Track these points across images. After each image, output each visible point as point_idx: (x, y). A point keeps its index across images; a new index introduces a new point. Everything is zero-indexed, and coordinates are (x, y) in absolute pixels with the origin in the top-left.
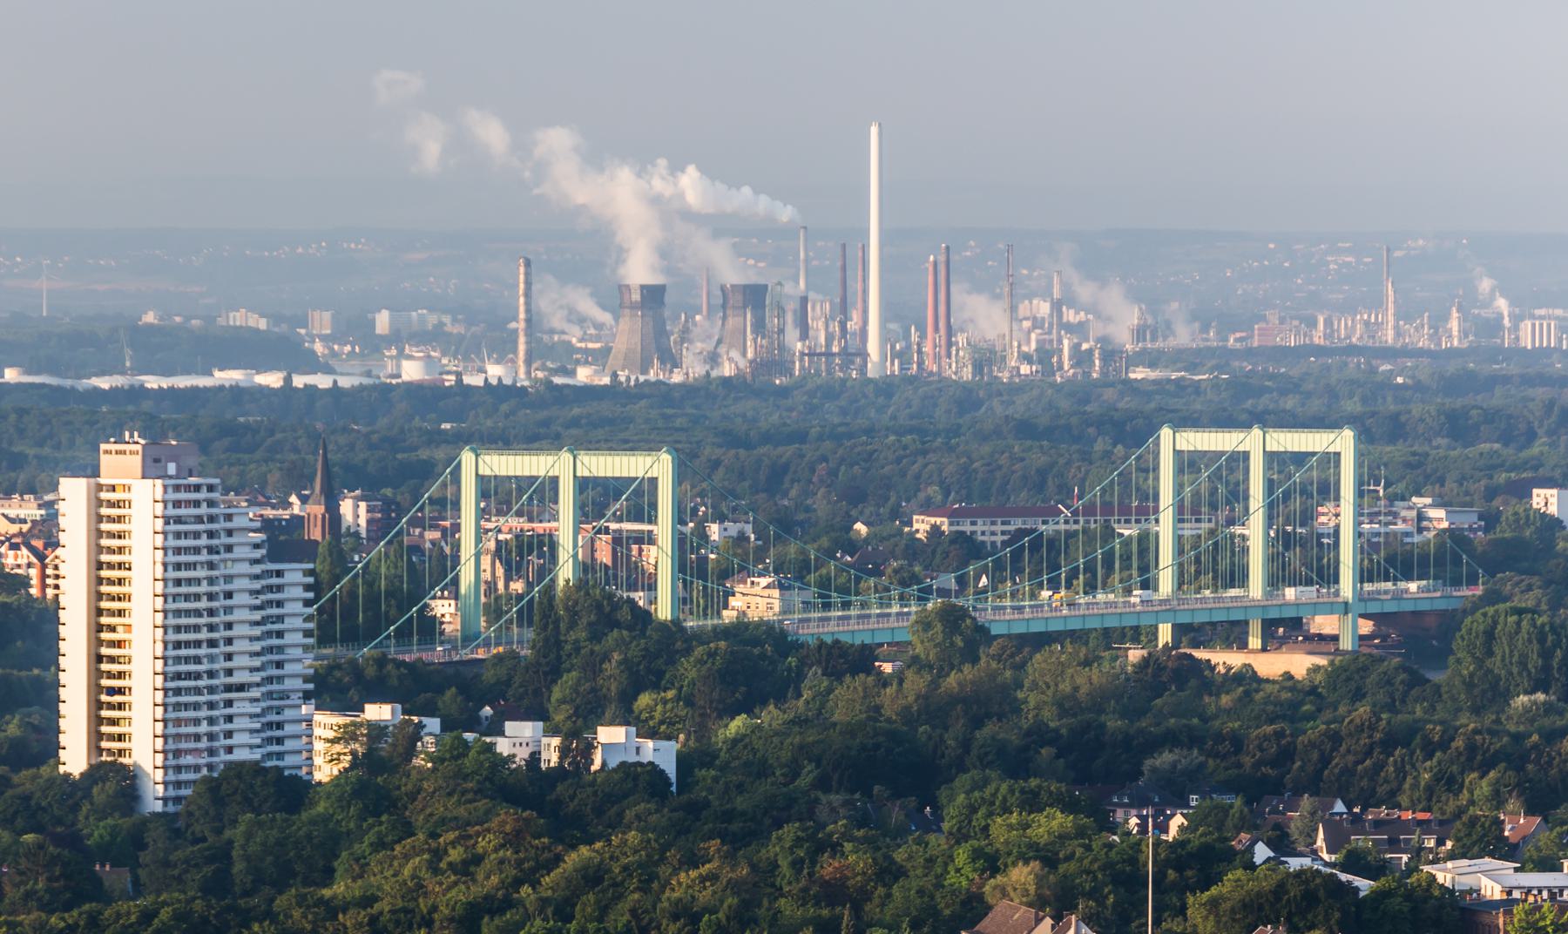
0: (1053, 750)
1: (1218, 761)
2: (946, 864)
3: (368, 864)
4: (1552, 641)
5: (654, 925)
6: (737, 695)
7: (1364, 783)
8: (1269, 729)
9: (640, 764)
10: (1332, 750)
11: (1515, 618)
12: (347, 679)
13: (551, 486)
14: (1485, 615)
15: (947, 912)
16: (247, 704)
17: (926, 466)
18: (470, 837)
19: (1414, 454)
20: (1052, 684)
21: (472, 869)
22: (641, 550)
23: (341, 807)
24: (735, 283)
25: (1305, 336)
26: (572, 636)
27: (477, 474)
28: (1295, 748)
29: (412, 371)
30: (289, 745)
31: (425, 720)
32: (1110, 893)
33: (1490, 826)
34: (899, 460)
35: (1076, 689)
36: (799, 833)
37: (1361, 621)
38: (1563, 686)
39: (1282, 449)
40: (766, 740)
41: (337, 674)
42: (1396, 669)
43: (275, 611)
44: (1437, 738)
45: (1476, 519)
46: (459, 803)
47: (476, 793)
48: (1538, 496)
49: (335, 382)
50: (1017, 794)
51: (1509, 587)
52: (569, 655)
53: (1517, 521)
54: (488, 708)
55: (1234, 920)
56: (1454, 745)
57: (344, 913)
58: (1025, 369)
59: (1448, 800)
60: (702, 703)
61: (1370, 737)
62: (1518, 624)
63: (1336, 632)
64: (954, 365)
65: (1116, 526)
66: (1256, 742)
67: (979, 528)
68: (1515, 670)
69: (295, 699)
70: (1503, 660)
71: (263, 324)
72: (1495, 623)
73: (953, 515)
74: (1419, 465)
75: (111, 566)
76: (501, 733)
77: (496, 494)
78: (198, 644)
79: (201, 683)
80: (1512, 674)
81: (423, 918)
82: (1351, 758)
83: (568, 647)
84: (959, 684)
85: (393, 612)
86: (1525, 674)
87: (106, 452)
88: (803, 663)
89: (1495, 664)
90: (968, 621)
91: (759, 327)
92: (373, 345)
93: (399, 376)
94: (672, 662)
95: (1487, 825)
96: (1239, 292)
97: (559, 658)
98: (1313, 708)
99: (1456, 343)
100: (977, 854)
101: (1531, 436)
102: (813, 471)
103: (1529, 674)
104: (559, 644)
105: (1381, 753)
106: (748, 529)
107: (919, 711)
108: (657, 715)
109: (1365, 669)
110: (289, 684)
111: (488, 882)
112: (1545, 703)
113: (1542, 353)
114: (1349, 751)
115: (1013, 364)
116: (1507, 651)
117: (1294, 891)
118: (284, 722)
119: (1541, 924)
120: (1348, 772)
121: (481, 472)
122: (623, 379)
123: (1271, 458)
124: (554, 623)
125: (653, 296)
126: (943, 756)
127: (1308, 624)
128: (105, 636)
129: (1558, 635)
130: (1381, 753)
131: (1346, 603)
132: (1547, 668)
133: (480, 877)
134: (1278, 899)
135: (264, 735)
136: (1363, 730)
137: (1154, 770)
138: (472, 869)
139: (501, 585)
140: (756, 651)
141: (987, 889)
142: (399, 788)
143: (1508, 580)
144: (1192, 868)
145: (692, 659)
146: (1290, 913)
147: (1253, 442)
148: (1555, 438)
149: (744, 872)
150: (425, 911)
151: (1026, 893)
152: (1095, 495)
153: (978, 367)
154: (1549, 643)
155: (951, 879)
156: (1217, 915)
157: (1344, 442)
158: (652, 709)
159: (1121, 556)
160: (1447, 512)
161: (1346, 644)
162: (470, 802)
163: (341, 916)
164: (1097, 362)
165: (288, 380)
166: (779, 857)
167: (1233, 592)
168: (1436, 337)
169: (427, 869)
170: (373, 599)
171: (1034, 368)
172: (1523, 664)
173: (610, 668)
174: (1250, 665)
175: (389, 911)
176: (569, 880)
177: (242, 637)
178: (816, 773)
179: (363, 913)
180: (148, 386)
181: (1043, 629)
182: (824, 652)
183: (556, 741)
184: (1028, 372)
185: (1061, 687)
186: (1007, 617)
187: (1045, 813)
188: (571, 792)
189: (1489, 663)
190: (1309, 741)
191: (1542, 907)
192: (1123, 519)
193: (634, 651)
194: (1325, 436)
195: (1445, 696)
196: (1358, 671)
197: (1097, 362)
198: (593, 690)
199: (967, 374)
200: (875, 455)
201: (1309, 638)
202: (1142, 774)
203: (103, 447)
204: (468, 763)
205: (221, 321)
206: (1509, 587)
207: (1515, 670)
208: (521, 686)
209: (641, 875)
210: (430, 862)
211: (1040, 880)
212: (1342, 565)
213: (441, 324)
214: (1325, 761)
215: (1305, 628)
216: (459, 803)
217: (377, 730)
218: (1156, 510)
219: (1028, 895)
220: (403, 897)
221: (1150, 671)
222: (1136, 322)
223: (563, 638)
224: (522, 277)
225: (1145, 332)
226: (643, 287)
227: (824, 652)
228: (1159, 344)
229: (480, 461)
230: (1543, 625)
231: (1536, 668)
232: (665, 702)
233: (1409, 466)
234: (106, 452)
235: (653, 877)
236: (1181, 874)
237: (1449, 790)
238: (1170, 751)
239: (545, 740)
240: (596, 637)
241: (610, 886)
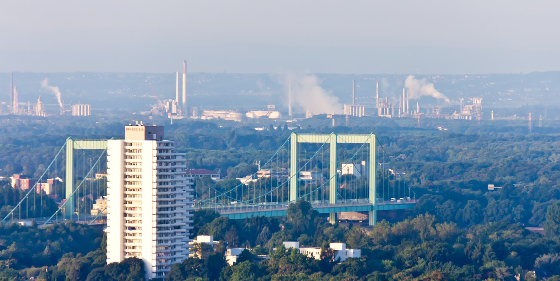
0: (516, 253)
16: (181, 234)
22: (41, 185)
23: (246, 275)
27: (73, 149)
39: (344, 142)
75: (130, 177)
78: (167, 209)
79: (168, 225)
87: (128, 129)
113: (82, 119)
121: (75, 148)
128: (128, 205)
131: (372, 206)
137: (540, 262)
147: (331, 139)
167: (366, 199)
177: (179, 207)
181: (233, 218)
182: (259, 221)
203: (126, 127)
227: (259, 221)
229: (75, 143)
234: (128, 129)
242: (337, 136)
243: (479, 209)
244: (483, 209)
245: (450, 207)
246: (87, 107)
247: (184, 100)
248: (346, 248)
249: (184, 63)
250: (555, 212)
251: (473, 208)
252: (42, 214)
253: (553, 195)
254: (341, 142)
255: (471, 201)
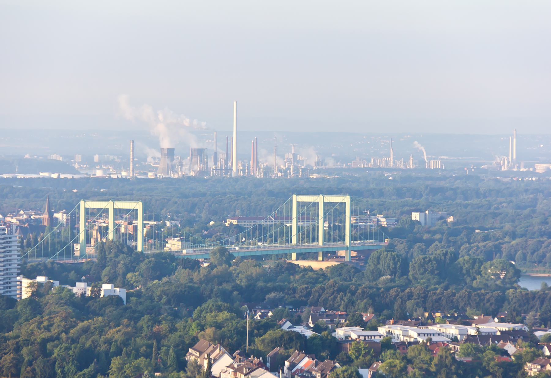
0: (238, 292)
1: (288, 296)
2: (190, 328)
3: (22, 326)
4: (397, 260)
5: (98, 345)
6: (157, 274)
7: (331, 303)
8: (304, 286)
9: (115, 296)
10: (322, 293)
11: (386, 253)
12: (42, 268)
13: (106, 211)
14: (377, 252)
15: (187, 342)
17: (237, 204)
18: (52, 318)
19: (382, 201)
20: (245, 272)
21: (50, 328)
24: (195, 148)
25: (366, 165)
26: (110, 256)
28: (311, 292)
29: (99, 173)
30: (13, 289)
31: (55, 282)
32: (235, 337)
33: (359, 317)
34: (229, 202)
35: (252, 274)
36: (149, 318)
37: (352, 252)
38: (400, 273)
40: (156, 288)
41: (39, 266)
42: (351, 268)
43: (8, 249)
44: (353, 289)
45: (395, 221)
46: (59, 306)
47: (64, 304)
48: (414, 214)
49: (73, 177)
50: (215, 307)
51: (396, 242)
52: (108, 262)
53: (404, 222)
54: (84, 277)
55: (269, 345)
56: (358, 291)
57: (9, 341)
58: (279, 174)
59: (351, 308)
60: (145, 276)
61: (333, 289)
62: (387, 255)
63: (344, 255)
64: (258, 173)
65: (284, 223)
66: (300, 290)
67: (246, 223)
68: (386, 268)
69: (15, 275)
70: (382, 265)
71: (61, 159)
72: (381, 254)
73: (239, 220)
74: (382, 205)
76: (75, 286)
77: (89, 213)
80: (385, 269)
81: (32, 342)
82: (328, 295)
83: (108, 259)
84: (217, 272)
85: (59, 248)
86: (389, 269)
88: (177, 265)
89: (380, 266)
90: (227, 253)
91: (201, 161)
92: (93, 165)
93: (96, 175)
94: (138, 264)
95: (358, 316)
96: (354, 151)
97: (105, 262)
98: (323, 280)
99: (411, 167)
100: (198, 325)
101: (421, 196)
102: (204, 205)
103: (390, 270)
104: (106, 258)
105: (336, 294)
106: (178, 223)
107: (204, 280)
108: (133, 280)
109: (342, 268)
110: (13, 271)
111: (54, 331)
112: (390, 279)
113: (436, 170)
114: (327, 293)
115: (276, 173)
116: (384, 262)
117: (286, 337)
118: (11, 282)
119: (360, 347)
120: (326, 299)
121: (86, 207)
122: (158, 176)
123: (325, 204)
124: (104, 252)
125: (171, 153)
126: (205, 294)
127: (337, 253)
129: (399, 258)
130: (336, 294)
131: (347, 247)
132: (395, 268)
133: (52, 330)
134: (281, 340)
135: (5, 286)
136: (331, 287)
137: (269, 298)
138: (50, 328)
139: (99, 239)
140: (164, 261)
141: (199, 335)
142: (42, 302)
143: (396, 241)
144: (262, 329)
145: (144, 263)
146: (285, 344)
147: (320, 199)
148: (428, 196)
149: (130, 329)
150: (33, 340)
151: (210, 337)
152: (70, 244)
153: (265, 173)
154: (396, 260)
155: (191, 332)
156: (264, 344)
157: (346, 199)
158: (131, 278)
159: (285, 232)
160: (386, 219)
161: (347, 259)
162: (62, 306)
163: (8, 342)
164: (300, 172)
165: (59, 176)
166: (143, 325)
167: (314, 243)
168: (405, 166)
169: (37, 328)
170: (53, 244)
171: (282, 174)
172: (388, 267)
173: (120, 266)
174: (310, 266)
175: (22, 340)
176: (78, 332)
178: (167, 298)
179: (14, 341)
180: (18, 177)
181: (260, 254)
182: (184, 261)
183: (90, 288)
184: (280, 175)
185: (248, 273)
186: (244, 251)
187: (222, 313)
188: (93, 304)
189: (378, 266)
190: (316, 290)
191: (360, 342)
192: (286, 221)
193: (127, 261)
194: (341, 197)
195: (365, 276)
196: (340, 268)
197: (300, 172)
198: (115, 272)
199: (262, 175)
200: (223, 201)
201: (337, 257)
202: (266, 299)
204: (63, 295)
205: (49, 158)
206: (396, 242)
207: (386, 268)
208: (94, 271)
209: (99, 330)
210: (37, 325)
211: (215, 333)
212: (346, 236)
213: (114, 159)
214: (320, 296)
215: (337, 254)
216: (59, 306)
217: (40, 285)
218: (291, 219)
219: (211, 337)
220: (27, 336)
221: (279, 267)
222: (316, 160)
223: (107, 256)
224: (131, 146)
225: (319, 163)
226: (168, 149)
227: (184, 261)
228: (323, 167)
230: (394, 255)
231: (392, 268)
232: (135, 276)
233: (379, 205)
235: (102, 331)
236: (259, 331)
237: (352, 305)
238: (274, 293)
239: (88, 288)
240: (116, 256)
241: (90, 333)
242: (298, 197)
243: (424, 249)
244: (427, 250)
245: (404, 248)
246: (438, 162)
247: (514, 157)
248: (115, 287)
249: (515, 131)
250: (374, 258)
251: (420, 249)
252: (42, 255)
253: (481, 239)
254: (299, 201)
255: (419, 243)
